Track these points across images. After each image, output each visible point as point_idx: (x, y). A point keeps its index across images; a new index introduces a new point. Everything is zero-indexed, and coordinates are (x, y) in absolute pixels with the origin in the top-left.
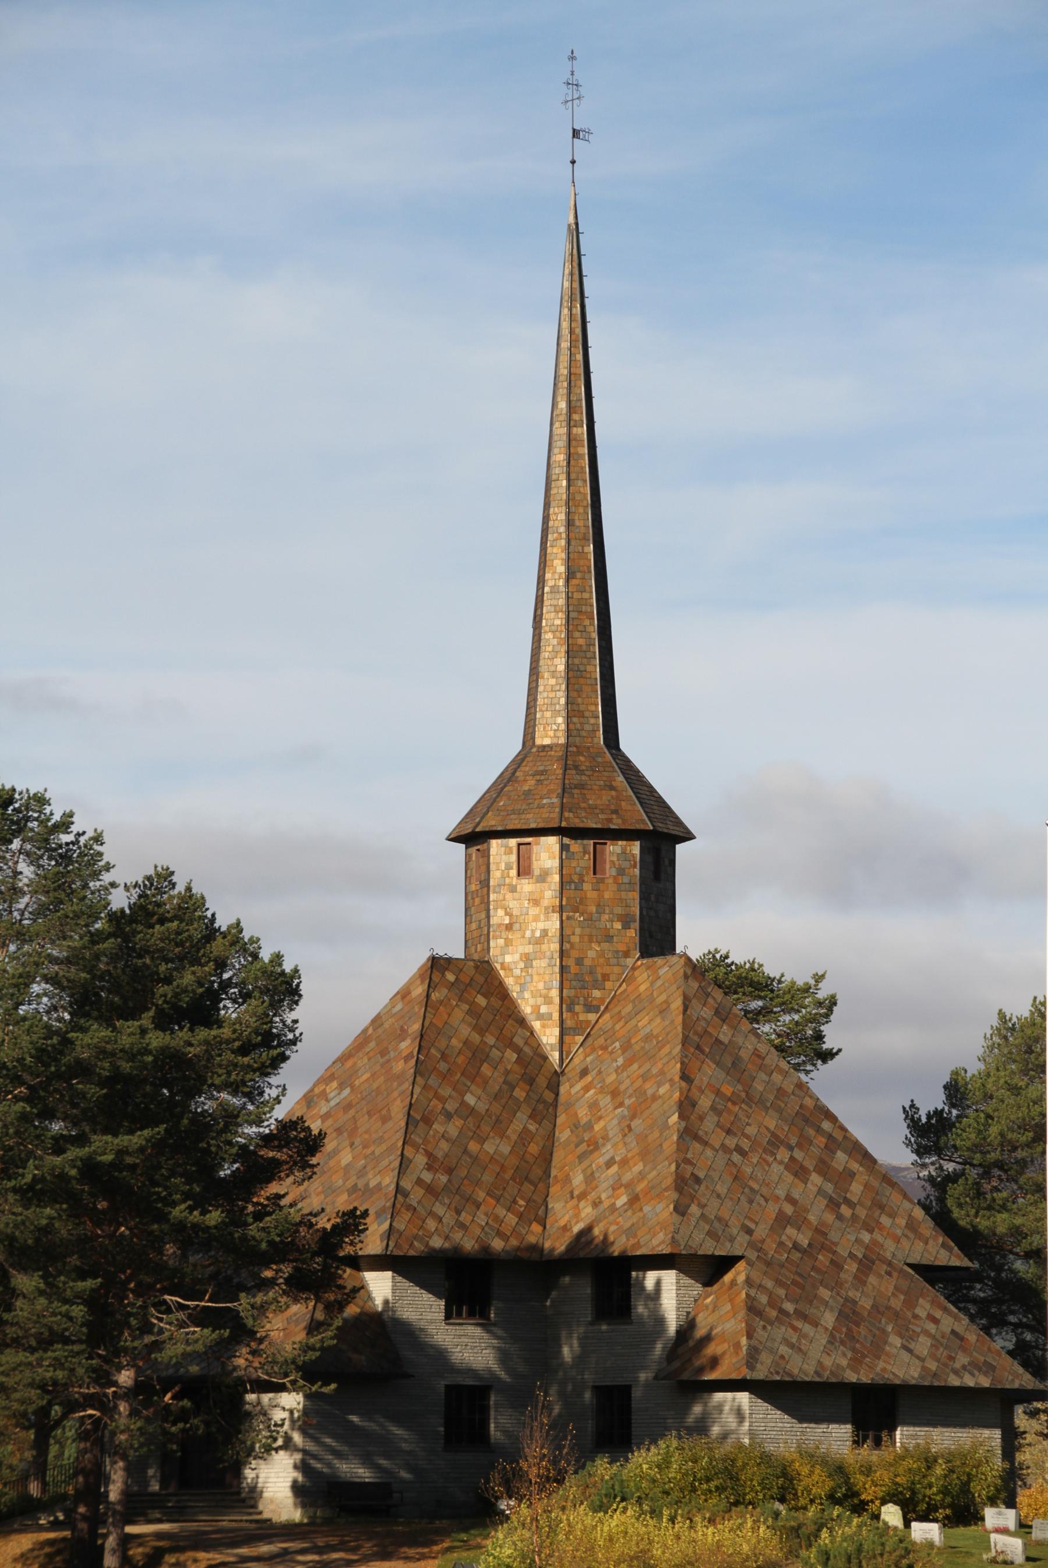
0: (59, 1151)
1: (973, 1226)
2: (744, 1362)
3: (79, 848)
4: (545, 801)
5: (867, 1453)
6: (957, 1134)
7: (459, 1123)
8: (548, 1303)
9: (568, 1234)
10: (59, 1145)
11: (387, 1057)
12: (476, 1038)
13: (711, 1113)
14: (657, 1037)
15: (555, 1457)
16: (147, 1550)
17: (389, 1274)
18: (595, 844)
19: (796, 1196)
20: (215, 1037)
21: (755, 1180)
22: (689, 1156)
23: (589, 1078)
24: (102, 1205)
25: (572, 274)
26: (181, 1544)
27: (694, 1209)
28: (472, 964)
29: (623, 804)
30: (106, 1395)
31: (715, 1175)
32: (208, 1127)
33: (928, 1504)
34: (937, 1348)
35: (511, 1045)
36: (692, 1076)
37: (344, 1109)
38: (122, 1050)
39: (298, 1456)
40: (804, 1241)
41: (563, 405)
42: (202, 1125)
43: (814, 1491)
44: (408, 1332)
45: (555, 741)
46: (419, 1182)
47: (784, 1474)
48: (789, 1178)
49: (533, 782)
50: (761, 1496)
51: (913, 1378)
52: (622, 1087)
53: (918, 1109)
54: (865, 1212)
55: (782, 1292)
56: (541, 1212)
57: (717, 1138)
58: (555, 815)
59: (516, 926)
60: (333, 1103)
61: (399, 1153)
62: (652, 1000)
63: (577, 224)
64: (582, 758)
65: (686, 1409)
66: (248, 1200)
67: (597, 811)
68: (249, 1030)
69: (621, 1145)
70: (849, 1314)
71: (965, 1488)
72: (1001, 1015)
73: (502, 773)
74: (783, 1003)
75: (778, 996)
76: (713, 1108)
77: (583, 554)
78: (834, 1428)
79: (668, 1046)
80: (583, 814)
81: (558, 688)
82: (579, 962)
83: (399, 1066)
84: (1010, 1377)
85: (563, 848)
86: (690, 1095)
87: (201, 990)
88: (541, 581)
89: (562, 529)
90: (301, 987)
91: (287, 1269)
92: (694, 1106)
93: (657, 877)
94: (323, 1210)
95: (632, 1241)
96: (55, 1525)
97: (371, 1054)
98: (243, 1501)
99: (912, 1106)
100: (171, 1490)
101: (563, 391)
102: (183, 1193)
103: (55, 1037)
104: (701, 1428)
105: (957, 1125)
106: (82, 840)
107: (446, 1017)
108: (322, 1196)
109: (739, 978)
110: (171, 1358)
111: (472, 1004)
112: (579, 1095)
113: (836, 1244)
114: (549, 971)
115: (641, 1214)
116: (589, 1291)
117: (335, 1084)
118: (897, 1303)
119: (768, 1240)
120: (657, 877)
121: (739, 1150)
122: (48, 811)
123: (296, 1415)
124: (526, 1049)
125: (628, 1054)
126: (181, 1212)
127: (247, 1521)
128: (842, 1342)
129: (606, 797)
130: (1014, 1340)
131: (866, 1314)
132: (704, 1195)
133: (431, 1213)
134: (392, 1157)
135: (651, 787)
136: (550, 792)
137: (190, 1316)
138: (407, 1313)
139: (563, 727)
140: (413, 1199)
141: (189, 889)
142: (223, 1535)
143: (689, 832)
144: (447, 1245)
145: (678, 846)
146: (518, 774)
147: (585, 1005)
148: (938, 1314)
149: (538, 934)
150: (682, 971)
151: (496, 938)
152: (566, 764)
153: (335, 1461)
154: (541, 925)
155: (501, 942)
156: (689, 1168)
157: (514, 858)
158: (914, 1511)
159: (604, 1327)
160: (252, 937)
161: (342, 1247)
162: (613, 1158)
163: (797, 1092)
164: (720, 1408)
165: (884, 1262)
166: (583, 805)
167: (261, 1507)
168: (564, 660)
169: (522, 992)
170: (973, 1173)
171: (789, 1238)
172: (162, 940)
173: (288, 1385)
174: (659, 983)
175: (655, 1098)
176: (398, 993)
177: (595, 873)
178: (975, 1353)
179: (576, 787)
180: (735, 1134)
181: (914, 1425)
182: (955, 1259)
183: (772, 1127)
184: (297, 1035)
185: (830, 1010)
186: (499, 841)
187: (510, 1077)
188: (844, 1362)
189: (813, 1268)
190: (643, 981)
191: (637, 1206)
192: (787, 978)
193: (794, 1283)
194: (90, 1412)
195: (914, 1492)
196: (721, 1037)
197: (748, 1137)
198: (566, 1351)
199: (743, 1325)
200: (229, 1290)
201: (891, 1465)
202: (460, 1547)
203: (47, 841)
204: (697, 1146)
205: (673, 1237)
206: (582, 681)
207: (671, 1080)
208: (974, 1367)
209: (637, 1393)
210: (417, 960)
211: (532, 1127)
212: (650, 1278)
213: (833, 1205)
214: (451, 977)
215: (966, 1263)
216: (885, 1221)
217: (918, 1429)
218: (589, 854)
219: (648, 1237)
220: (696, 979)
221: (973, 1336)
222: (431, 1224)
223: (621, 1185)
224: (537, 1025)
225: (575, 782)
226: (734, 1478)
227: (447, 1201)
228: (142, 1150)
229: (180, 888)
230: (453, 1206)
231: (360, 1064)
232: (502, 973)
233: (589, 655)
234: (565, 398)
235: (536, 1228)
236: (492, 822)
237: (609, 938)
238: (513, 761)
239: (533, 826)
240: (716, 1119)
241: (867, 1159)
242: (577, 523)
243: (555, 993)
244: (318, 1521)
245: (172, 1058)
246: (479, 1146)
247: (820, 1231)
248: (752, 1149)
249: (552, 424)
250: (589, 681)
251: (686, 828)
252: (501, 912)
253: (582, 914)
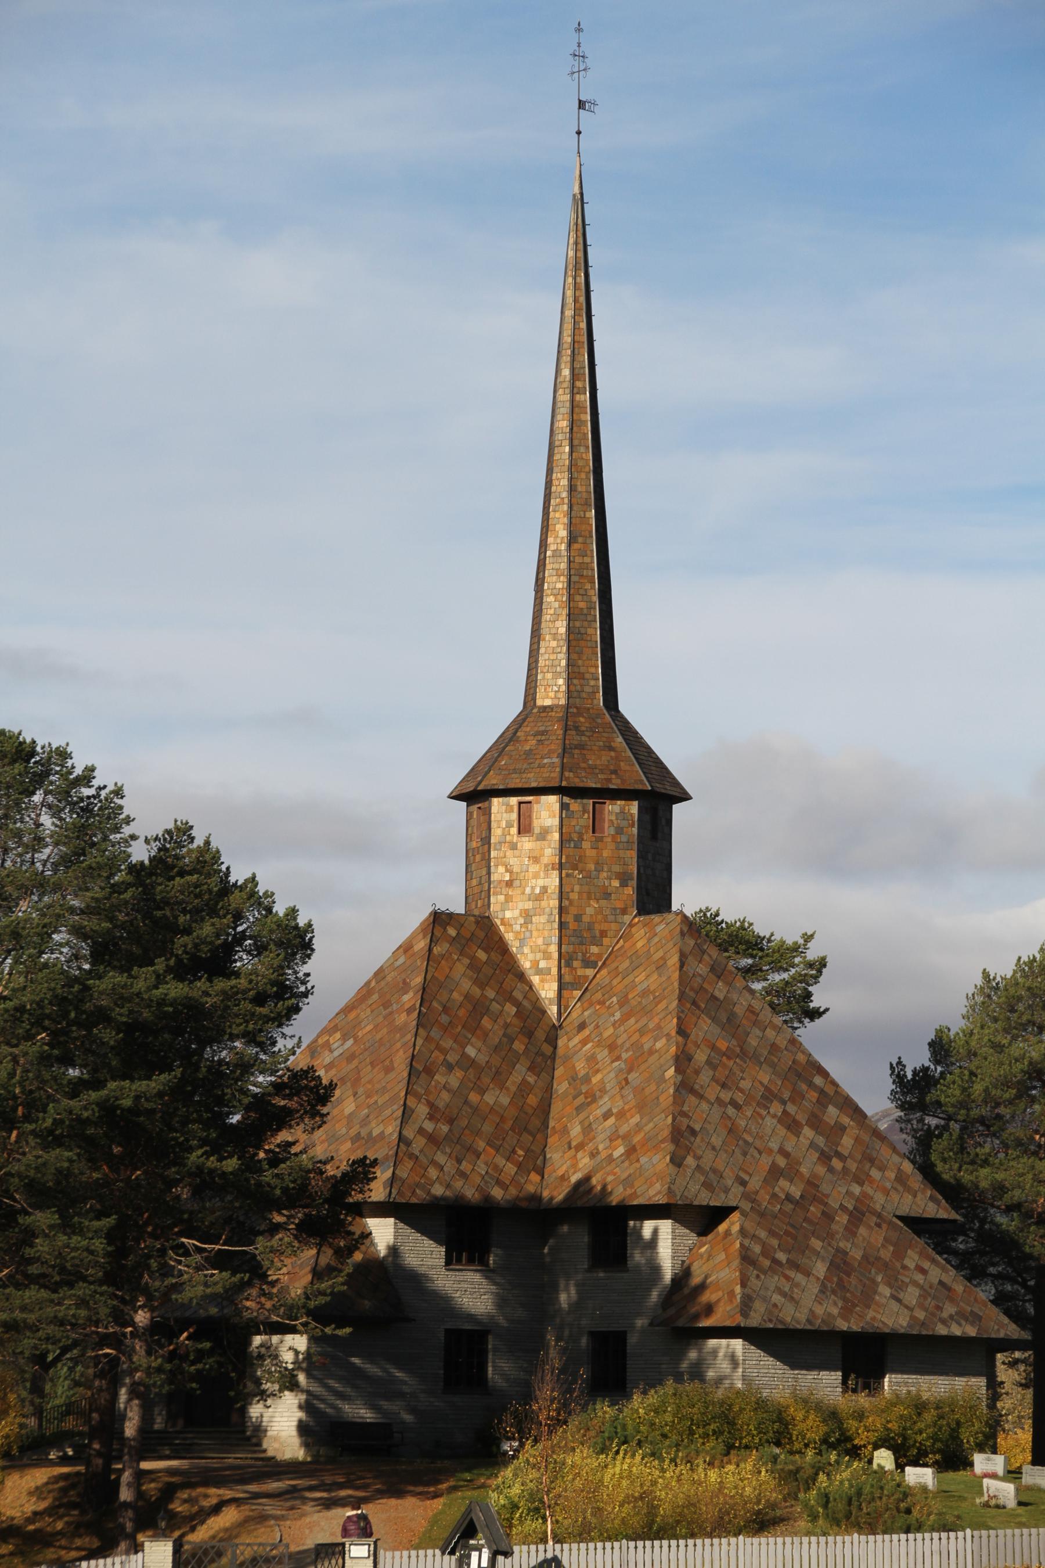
0: (74, 1095)
1: (956, 1179)
2: (738, 1310)
3: (100, 801)
4: (545, 761)
5: (862, 1400)
6: (941, 1091)
8: (546, 1251)
9: (566, 1183)
10: (76, 1089)
11: (390, 1009)
12: (477, 992)
13: (706, 1067)
14: (654, 991)
15: (566, 1399)
16: (160, 1485)
17: (392, 1220)
18: (594, 803)
19: (790, 1149)
20: (232, 988)
21: (750, 1133)
22: (686, 1108)
23: (586, 1032)
24: (116, 1150)
25: (576, 243)
27: (690, 1161)
28: (472, 919)
29: (622, 764)
30: (124, 1335)
32: (221, 1075)
33: (919, 1449)
34: (925, 1298)
36: (689, 1031)
39: (303, 1397)
40: (796, 1192)
41: (566, 372)
44: (416, 1280)
45: (556, 702)
46: (421, 1131)
47: (780, 1419)
48: (782, 1131)
49: (534, 742)
51: (902, 1327)
52: (619, 1042)
55: (775, 1242)
56: (539, 1162)
57: (713, 1092)
59: (517, 883)
60: (336, 1053)
61: (402, 1102)
62: (649, 956)
63: (582, 194)
64: (582, 719)
65: (682, 1354)
66: (259, 1147)
67: (597, 771)
69: (618, 1097)
70: (840, 1264)
72: (986, 974)
73: (504, 733)
75: (767, 955)
76: (709, 1062)
77: (585, 519)
78: (824, 1375)
80: (583, 774)
81: (559, 650)
82: (578, 918)
83: (401, 1018)
84: (996, 1327)
85: (564, 807)
88: (543, 545)
89: (565, 495)
92: (690, 1060)
93: (654, 837)
95: (629, 1191)
96: (64, 1460)
97: (374, 1006)
98: (249, 1439)
99: (899, 1063)
101: (566, 358)
102: (200, 1139)
104: (697, 1373)
106: (103, 794)
107: (448, 970)
108: (326, 1144)
109: (730, 936)
110: (191, 1299)
111: (473, 958)
112: (577, 1049)
113: (827, 1196)
114: (548, 927)
115: (638, 1165)
116: (586, 1239)
117: (338, 1035)
118: (886, 1254)
119: (762, 1191)
120: (654, 837)
121: (733, 1103)
122: (69, 764)
123: (301, 1357)
124: (525, 1003)
125: (625, 1009)
127: (251, 1458)
128: (834, 1292)
130: (993, 1291)
131: (856, 1264)
133: (433, 1162)
134: (395, 1107)
135: (650, 748)
136: (551, 752)
137: (206, 1259)
139: (564, 688)
141: (207, 843)
143: (686, 793)
144: (448, 1193)
145: (674, 806)
146: (519, 734)
147: (583, 961)
148: (926, 1265)
149: (537, 891)
150: (678, 929)
151: (497, 894)
152: (566, 725)
153: (338, 1402)
154: (541, 882)
155: (501, 898)
156: (685, 1121)
157: (514, 816)
158: (905, 1456)
159: (601, 1275)
160: (267, 892)
162: (610, 1110)
163: (790, 1047)
164: (715, 1352)
166: (583, 765)
167: (265, 1446)
168: (565, 623)
169: (521, 946)
170: (955, 1127)
171: (782, 1190)
172: (182, 892)
173: (300, 1328)
174: (656, 939)
175: (651, 1052)
176: (400, 946)
177: (594, 832)
179: (576, 747)
180: (730, 1089)
181: (903, 1372)
183: (766, 1081)
186: (501, 799)
187: (509, 1030)
188: (835, 1311)
189: (805, 1219)
190: (640, 935)
191: (633, 1157)
192: (777, 937)
193: (787, 1233)
195: (905, 1439)
196: (717, 993)
197: (741, 1091)
198: (563, 1297)
199: (737, 1274)
200: (248, 1235)
201: (883, 1411)
203: (68, 793)
204: (692, 1099)
205: (669, 1188)
206: (582, 643)
207: (668, 1035)
208: (962, 1316)
209: (632, 1340)
210: (418, 916)
211: (531, 1079)
212: (648, 1227)
213: (825, 1157)
214: (452, 932)
215: (954, 1215)
216: (875, 1174)
217: (906, 1376)
218: (588, 813)
219: (645, 1187)
221: (959, 1287)
222: (433, 1173)
223: (619, 1137)
224: (535, 980)
225: (576, 742)
226: (732, 1423)
227: (448, 1150)
228: (160, 1094)
229: (199, 842)
231: (363, 1016)
232: (502, 928)
233: (589, 618)
235: (534, 1177)
236: (493, 781)
237: (607, 896)
238: (514, 721)
239: (534, 785)
240: (711, 1073)
242: (579, 489)
243: (554, 949)
244: (322, 1459)
245: (192, 1009)
246: (479, 1097)
247: (812, 1183)
248: (747, 1103)
249: (555, 391)
250: (589, 644)
252: (501, 869)
253: (581, 872)
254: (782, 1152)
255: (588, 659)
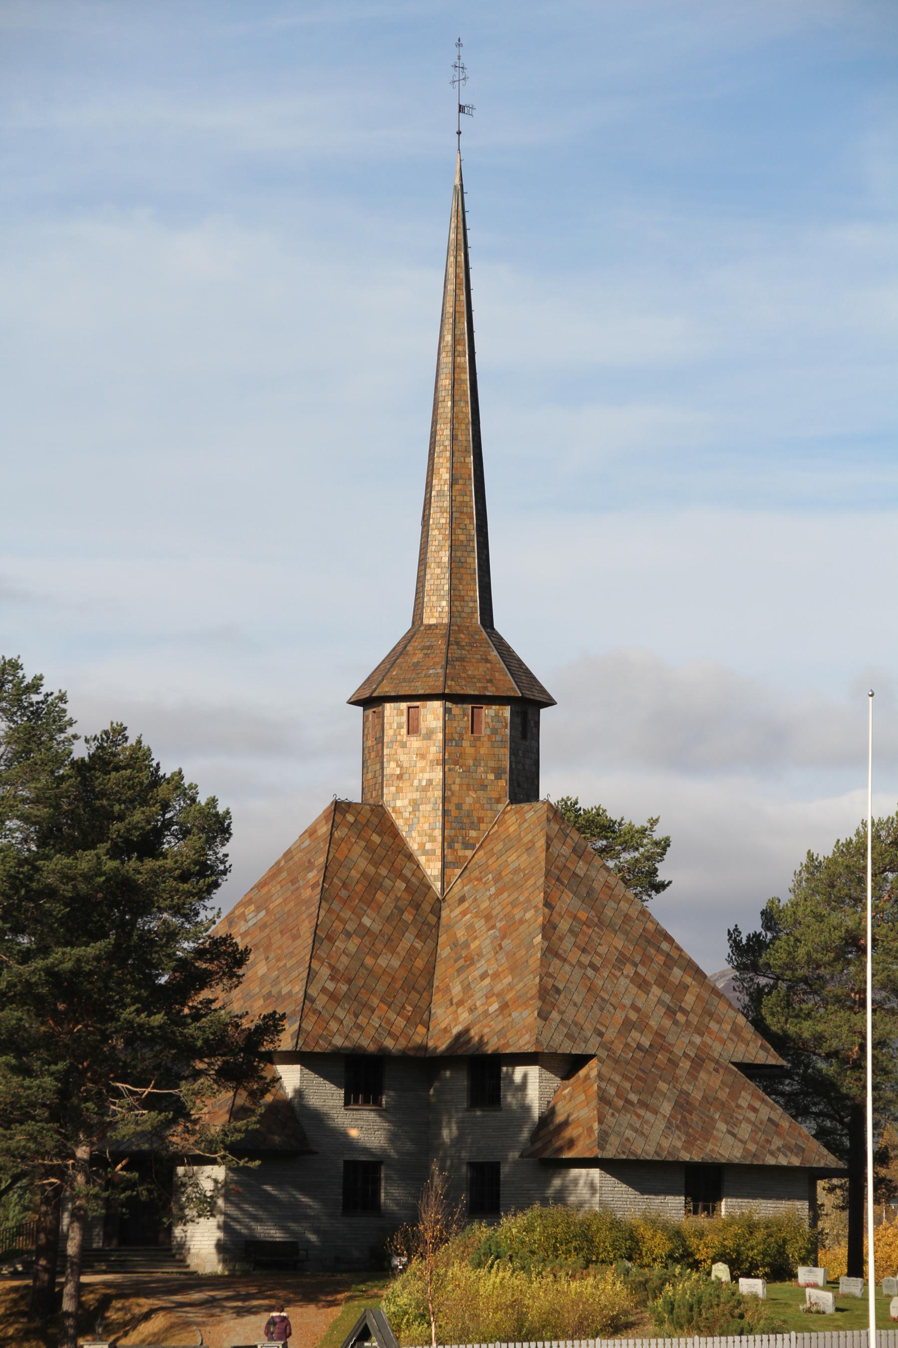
2: (596, 1143)
4: (431, 671)
5: (702, 1220)
6: (770, 954)
7: (357, 940)
9: (448, 1035)
10: (26, 957)
11: (297, 885)
12: (371, 870)
14: (524, 869)
15: (448, 1221)
16: (97, 1296)
17: (298, 1067)
19: (640, 1005)
20: (160, 867)
21: (606, 991)
22: (551, 970)
23: (466, 905)
24: (61, 1007)
25: (457, 227)
26: (126, 1292)
27: (555, 1015)
28: (368, 807)
29: (497, 674)
30: (67, 1166)
31: (573, 987)
32: (152, 942)
33: (751, 1263)
34: (756, 1133)
35: (401, 876)
37: (260, 928)
38: (80, 875)
39: (220, 1218)
40: (646, 1043)
41: (448, 338)
42: (147, 939)
43: (656, 1251)
44: (318, 1118)
45: (440, 621)
46: (324, 990)
47: (632, 1238)
48: (634, 990)
49: (421, 655)
50: (612, 1256)
51: (736, 1158)
52: (494, 913)
53: (740, 933)
54: (697, 1019)
55: (628, 1085)
56: (425, 1017)
58: (440, 683)
59: (406, 776)
60: (251, 923)
61: (307, 965)
62: (520, 839)
63: (462, 186)
64: (462, 636)
65: (547, 1183)
66: (183, 1004)
68: (188, 861)
69: (493, 961)
70: (683, 1104)
71: (781, 1250)
72: (810, 855)
73: (395, 648)
74: (626, 842)
76: (571, 930)
79: (533, 878)
80: (464, 683)
82: (459, 807)
83: (307, 893)
84: (817, 1158)
85: (446, 711)
86: (552, 919)
87: (149, 827)
88: (429, 486)
89: (447, 443)
90: (232, 826)
91: (218, 1062)
92: (555, 929)
93: (524, 736)
94: (247, 1013)
95: (502, 1042)
96: (15, 1275)
97: (283, 883)
99: (736, 930)
100: (112, 1247)
101: (449, 326)
102: (133, 997)
103: (26, 866)
104: (560, 1197)
105: (771, 946)
107: (347, 852)
108: (242, 1002)
109: (587, 820)
111: (368, 841)
113: (673, 1045)
114: (433, 814)
115: (510, 1019)
116: (465, 1083)
117: (252, 907)
118: (723, 1095)
119: (616, 1041)
120: (524, 736)
121: (592, 966)
122: (20, 674)
124: (413, 880)
126: (130, 1014)
127: (177, 1273)
128: (678, 1128)
129: (482, 668)
131: (697, 1104)
132: (563, 1003)
133: (334, 1017)
134: (301, 969)
136: (435, 664)
138: (314, 1100)
139: (447, 609)
140: (319, 1005)
141: (139, 742)
142: (161, 1285)
143: (551, 699)
145: (542, 711)
146: (408, 648)
147: (463, 843)
148: (757, 1104)
149: (424, 783)
150: (545, 815)
151: (388, 786)
153: (252, 1224)
154: (427, 776)
155: (393, 789)
156: (551, 981)
157: (404, 719)
158: (739, 1269)
159: (478, 1113)
160: (191, 784)
161: (263, 1045)
162: (486, 972)
163: (641, 917)
164: (575, 1182)
165: (712, 1061)
167: (189, 1262)
168: (448, 553)
169: (410, 831)
170: (783, 986)
172: (117, 785)
173: (219, 1160)
174: (526, 825)
175: (522, 921)
176: (306, 831)
177: (472, 733)
178: (787, 1138)
180: (589, 953)
181: (737, 1197)
182: (768, 1057)
183: (620, 947)
184: (227, 866)
185: (665, 849)
186: (392, 704)
187: (400, 903)
188: (679, 1144)
191: (506, 1012)
192: (626, 821)
194: (53, 1180)
195: (739, 1254)
196: (578, 871)
197: (600, 955)
198: (445, 1133)
199: (595, 1112)
200: (173, 1080)
202: (362, 1296)
204: (557, 962)
205: (537, 1039)
206: (463, 571)
207: (536, 907)
208: (787, 1149)
209: (505, 1170)
211: (418, 945)
212: (519, 1072)
213: (671, 1012)
215: (782, 1062)
216: (714, 1026)
217: (740, 1200)
220: (557, 822)
221: (786, 1122)
222: (334, 1026)
223: (493, 995)
224: (422, 859)
225: (457, 656)
227: (347, 1006)
228: (98, 958)
229: (132, 741)
230: (352, 1010)
231: (273, 890)
232: (393, 815)
233: (469, 549)
234: (451, 332)
235: (421, 1029)
236: (387, 689)
237: (484, 787)
239: (421, 692)
240: (573, 940)
241: (698, 973)
242: (460, 438)
243: (438, 833)
244: (238, 1273)
246: (374, 961)
247: (659, 1034)
249: (439, 354)
251: (549, 695)
252: (393, 765)
253: (461, 767)
254: (634, 1007)
255: (467, 584)
